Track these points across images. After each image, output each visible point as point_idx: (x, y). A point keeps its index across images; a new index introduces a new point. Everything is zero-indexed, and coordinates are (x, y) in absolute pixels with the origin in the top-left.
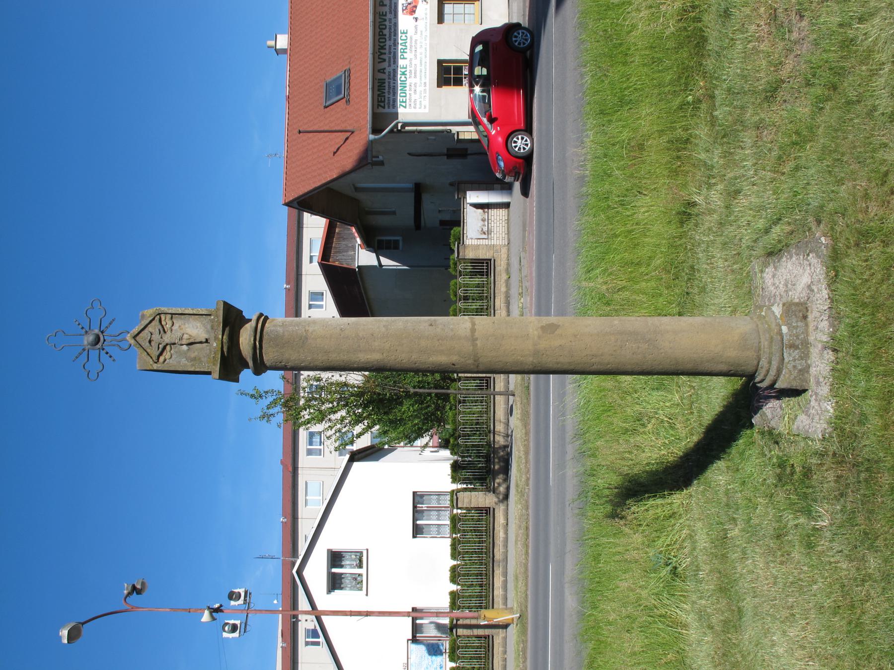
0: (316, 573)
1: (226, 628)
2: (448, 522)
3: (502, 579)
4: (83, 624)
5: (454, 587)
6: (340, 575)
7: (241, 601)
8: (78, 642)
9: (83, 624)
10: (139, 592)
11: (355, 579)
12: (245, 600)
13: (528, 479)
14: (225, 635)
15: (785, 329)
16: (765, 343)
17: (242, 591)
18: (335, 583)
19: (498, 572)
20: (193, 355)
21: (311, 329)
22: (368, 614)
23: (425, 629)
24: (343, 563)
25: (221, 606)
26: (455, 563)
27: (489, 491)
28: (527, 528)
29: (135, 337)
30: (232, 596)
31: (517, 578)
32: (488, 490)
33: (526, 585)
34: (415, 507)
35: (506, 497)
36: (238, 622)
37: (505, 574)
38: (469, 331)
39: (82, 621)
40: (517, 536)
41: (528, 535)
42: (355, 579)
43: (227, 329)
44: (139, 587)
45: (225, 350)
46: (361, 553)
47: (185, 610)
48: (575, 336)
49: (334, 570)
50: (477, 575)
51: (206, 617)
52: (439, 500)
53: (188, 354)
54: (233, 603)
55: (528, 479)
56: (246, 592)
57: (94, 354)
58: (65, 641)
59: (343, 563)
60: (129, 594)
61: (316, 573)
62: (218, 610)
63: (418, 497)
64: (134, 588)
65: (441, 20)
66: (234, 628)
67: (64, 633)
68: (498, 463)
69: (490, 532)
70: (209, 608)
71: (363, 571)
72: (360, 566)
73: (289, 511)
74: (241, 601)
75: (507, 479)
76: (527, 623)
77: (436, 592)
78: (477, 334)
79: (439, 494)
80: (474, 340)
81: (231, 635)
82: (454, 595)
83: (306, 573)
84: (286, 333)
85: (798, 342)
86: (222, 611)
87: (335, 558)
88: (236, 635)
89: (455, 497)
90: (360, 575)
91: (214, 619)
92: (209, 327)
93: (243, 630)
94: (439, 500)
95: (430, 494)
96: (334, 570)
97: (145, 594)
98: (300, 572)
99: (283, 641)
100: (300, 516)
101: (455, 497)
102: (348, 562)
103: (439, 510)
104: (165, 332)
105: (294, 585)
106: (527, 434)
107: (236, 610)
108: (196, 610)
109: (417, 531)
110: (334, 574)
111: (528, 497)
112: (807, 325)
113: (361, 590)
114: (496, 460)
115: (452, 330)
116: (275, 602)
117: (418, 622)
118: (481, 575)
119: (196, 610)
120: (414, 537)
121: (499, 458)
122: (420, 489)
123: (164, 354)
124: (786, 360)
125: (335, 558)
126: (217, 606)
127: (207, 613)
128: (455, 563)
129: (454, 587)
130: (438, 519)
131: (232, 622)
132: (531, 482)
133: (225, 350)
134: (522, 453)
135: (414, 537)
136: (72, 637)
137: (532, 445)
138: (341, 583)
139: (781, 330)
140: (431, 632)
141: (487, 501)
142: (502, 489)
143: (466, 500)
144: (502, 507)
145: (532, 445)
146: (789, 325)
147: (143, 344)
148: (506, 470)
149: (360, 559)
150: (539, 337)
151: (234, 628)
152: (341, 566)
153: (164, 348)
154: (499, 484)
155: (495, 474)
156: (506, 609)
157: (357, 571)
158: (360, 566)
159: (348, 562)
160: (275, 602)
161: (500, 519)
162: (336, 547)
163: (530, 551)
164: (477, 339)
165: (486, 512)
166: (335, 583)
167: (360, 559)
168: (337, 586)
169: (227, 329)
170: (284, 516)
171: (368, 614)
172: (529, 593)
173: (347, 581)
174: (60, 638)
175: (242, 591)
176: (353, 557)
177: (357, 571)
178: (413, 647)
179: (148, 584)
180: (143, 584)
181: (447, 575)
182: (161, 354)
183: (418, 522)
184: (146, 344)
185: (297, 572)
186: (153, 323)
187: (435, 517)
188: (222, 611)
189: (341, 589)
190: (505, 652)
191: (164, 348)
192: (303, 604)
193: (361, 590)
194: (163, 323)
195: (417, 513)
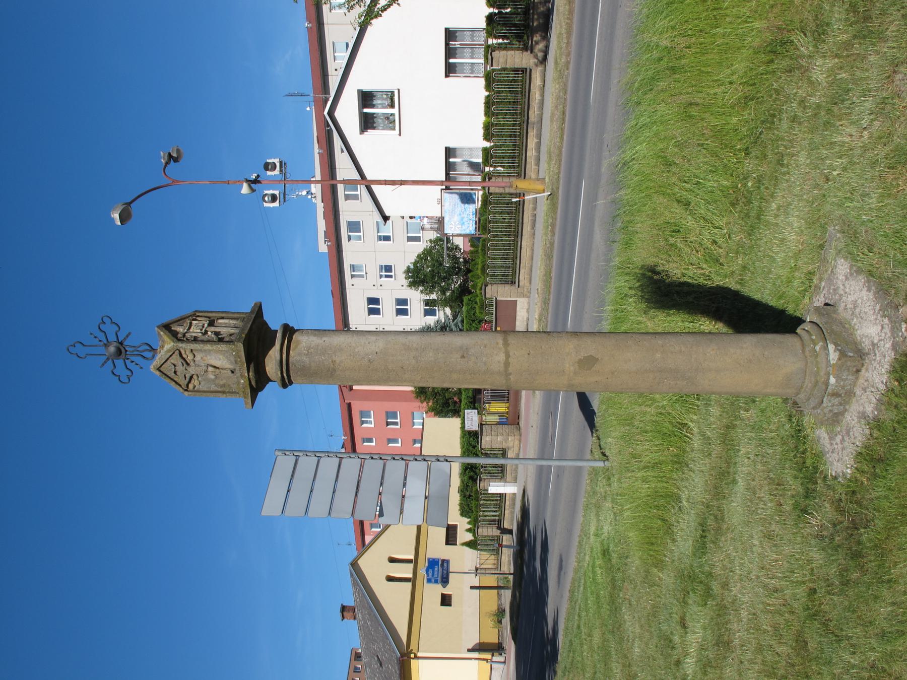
0: (348, 113)
1: (266, 199)
2: (482, 61)
3: (535, 140)
4: (131, 203)
5: (487, 144)
6: (372, 115)
7: (277, 172)
8: (129, 224)
9: (131, 203)
10: (176, 160)
11: (388, 118)
12: (281, 170)
13: (568, 63)
14: (266, 205)
15: (832, 380)
16: (808, 384)
17: (277, 161)
18: (367, 123)
19: (532, 134)
20: (221, 383)
21: (338, 360)
22: (402, 183)
23: (458, 167)
24: (375, 102)
25: (258, 176)
26: (491, 10)
27: (526, 50)
28: (564, 113)
29: (159, 369)
30: (267, 167)
31: (550, 154)
32: (525, 48)
33: (560, 165)
34: (447, 44)
35: (545, 59)
36: (276, 192)
37: (539, 136)
38: (502, 365)
39: (129, 201)
40: (553, 115)
41: (564, 120)
42: (388, 118)
43: (252, 366)
44: (175, 155)
45: (253, 383)
46: (393, 93)
47: (224, 182)
48: (613, 373)
49: (366, 110)
50: (510, 136)
51: (245, 189)
52: (472, 36)
53: (217, 381)
54: (269, 173)
55: (568, 63)
56: (281, 163)
57: (119, 362)
58: (119, 223)
59: (375, 102)
60: (167, 164)
61: (348, 113)
62: (256, 181)
63: (450, 35)
64: (170, 156)
65: (472, 588)
66: (274, 198)
67: (116, 216)
68: (537, 19)
69: (526, 93)
70: (247, 181)
71: (395, 111)
72: (392, 106)
73: (314, 16)
74: (277, 172)
75: (546, 37)
76: (557, 203)
77: (472, 139)
78: (510, 369)
79: (473, 31)
80: (507, 374)
81: (272, 205)
82: (490, 18)
83: (338, 114)
84: (313, 364)
85: (842, 392)
86: (259, 182)
87: (366, 98)
88: (276, 204)
89: (490, 57)
90: (392, 115)
91: (253, 190)
92: (232, 359)
93: (282, 200)
94: (472, 36)
95: (463, 31)
96: (366, 110)
97: (182, 161)
98: (331, 113)
99: (320, 147)
100: (325, 22)
101: (490, 57)
102: (379, 102)
103: (472, 47)
104: (188, 364)
105: (329, 131)
106: (571, 12)
107: (273, 182)
108: (235, 182)
109: (450, 70)
110: (366, 114)
111: (567, 81)
112: (857, 378)
113: (394, 129)
114: (536, 17)
115: (485, 364)
116: (308, 109)
117: (451, 160)
118: (515, 136)
119: (235, 182)
120: (447, 76)
121: (538, 14)
122: (452, 25)
123: (193, 381)
124: (824, 405)
125: (366, 98)
126: (253, 177)
127: (245, 185)
128: (491, 10)
129: (487, 144)
130: (472, 58)
131: (271, 192)
132: (571, 66)
133: (253, 383)
134: (564, 31)
135: (447, 76)
136: (125, 217)
137: (575, 27)
138: (374, 123)
139: (829, 379)
140: (463, 172)
141: (524, 61)
142: (541, 46)
143: (501, 60)
144: (540, 69)
145: (575, 27)
146: (838, 378)
147: (168, 374)
148: (546, 28)
149: (391, 99)
150: (575, 373)
151: (274, 198)
152: (373, 106)
153: (191, 377)
154: (537, 43)
155: (533, 32)
156: (538, 180)
157: (389, 111)
158: (392, 106)
159: (379, 102)
160: (308, 109)
161: (537, 80)
162: (366, 88)
163: (565, 137)
164: (510, 374)
165: (523, 73)
166: (367, 123)
167: (391, 99)
168: (370, 125)
169: (252, 366)
170: (309, 19)
171: (402, 183)
172: (561, 176)
173: (379, 121)
174: (113, 220)
175: (277, 161)
176: (385, 96)
177: (389, 111)
178: (446, 196)
179: (182, 150)
180: (178, 151)
181: (481, 132)
182: (190, 382)
183: (451, 160)
184: (172, 375)
185: (328, 113)
186: (174, 356)
187: (468, 55)
188: (259, 182)
189: (374, 128)
190: (535, 209)
191: (191, 377)
192: (338, 143)
193: (394, 129)
194: (184, 356)
195: (450, 52)
